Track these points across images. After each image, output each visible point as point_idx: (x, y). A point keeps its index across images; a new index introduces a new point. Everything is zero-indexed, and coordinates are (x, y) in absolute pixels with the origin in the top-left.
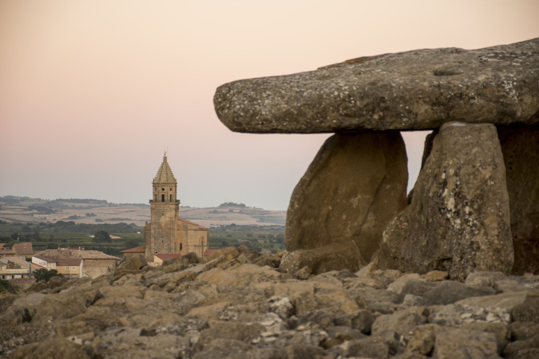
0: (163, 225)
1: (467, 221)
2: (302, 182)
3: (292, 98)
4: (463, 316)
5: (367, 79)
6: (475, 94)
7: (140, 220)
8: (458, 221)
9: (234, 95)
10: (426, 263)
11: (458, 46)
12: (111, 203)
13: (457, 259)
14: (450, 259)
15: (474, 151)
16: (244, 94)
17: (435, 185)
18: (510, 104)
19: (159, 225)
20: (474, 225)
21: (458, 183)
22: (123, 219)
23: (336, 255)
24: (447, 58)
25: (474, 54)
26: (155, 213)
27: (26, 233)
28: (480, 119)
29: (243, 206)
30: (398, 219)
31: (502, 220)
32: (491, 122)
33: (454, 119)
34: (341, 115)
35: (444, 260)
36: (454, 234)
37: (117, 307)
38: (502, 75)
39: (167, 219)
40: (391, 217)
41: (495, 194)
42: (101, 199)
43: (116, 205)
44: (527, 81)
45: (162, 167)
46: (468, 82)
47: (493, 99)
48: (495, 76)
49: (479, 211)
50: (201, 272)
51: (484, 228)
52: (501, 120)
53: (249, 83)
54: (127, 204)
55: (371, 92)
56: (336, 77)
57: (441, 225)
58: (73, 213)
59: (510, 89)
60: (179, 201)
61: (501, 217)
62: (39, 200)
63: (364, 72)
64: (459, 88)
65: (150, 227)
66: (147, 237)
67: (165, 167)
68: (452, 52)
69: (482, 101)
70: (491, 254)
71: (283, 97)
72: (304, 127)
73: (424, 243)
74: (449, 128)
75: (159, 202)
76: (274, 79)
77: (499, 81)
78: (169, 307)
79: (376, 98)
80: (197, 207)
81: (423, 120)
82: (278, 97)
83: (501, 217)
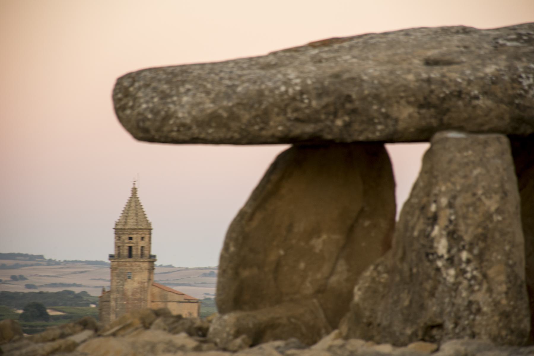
0: (129, 293)
1: (464, 272)
2: (242, 214)
3: (221, 95)
5: (330, 68)
6: (480, 93)
7: (94, 285)
8: (452, 272)
9: (139, 88)
10: (409, 331)
12: (50, 260)
13: (449, 325)
14: (440, 326)
15: (476, 172)
18: (529, 107)
19: (124, 294)
21: (453, 218)
22: (69, 285)
24: (449, 40)
25: (488, 35)
26: (118, 276)
28: (486, 128)
31: (513, 271)
33: (449, 127)
34: (289, 119)
35: (432, 327)
36: (446, 289)
38: (520, 66)
39: (136, 285)
40: (365, 268)
41: (503, 234)
42: (36, 253)
43: (58, 263)
45: (129, 204)
46: (470, 74)
50: (84, 341)
51: (488, 282)
53: (161, 72)
54: (76, 261)
55: (332, 88)
56: (286, 65)
57: (429, 277)
60: (154, 256)
61: (511, 266)
63: (327, 60)
64: (457, 84)
65: (109, 297)
66: (104, 313)
67: (134, 204)
68: (457, 32)
70: (497, 318)
71: (208, 93)
72: (237, 136)
73: (406, 303)
75: (124, 258)
76: (198, 67)
77: (513, 74)
79: (340, 96)
80: (184, 265)
82: (201, 92)
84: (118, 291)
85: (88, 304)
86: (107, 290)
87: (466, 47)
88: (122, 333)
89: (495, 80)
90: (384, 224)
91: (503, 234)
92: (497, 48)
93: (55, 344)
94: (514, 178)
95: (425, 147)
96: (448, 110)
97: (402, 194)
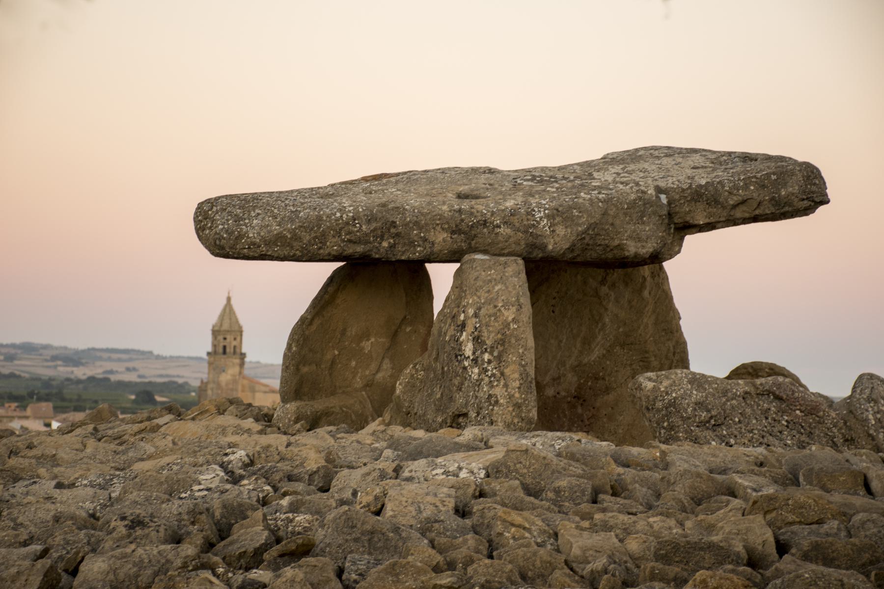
0: (223, 384)
1: (487, 371)
2: (303, 319)
4: (434, 472)
5: (378, 199)
7: (195, 376)
8: (476, 370)
9: (217, 212)
10: (440, 419)
11: (492, 166)
13: (473, 414)
14: (465, 415)
15: (497, 288)
16: (229, 212)
17: (452, 328)
19: (219, 385)
20: (493, 375)
22: (174, 376)
23: (341, 408)
25: (509, 175)
26: (214, 369)
27: (47, 391)
28: (506, 251)
30: (414, 367)
32: (519, 256)
33: (476, 250)
34: (343, 241)
35: (459, 416)
37: (45, 459)
38: (533, 201)
40: (407, 366)
43: (165, 358)
44: (560, 209)
45: (224, 310)
47: (522, 229)
48: (525, 202)
49: (499, 358)
52: (530, 253)
55: (380, 215)
57: (457, 375)
58: (109, 366)
59: (541, 218)
61: (523, 366)
62: (66, 348)
63: (376, 192)
64: (483, 215)
65: (206, 386)
67: (228, 310)
68: (484, 172)
69: (508, 231)
70: (511, 409)
72: (298, 253)
73: (438, 396)
74: (471, 260)
78: (109, 461)
79: (386, 222)
81: (441, 251)
83: (523, 366)
84: (214, 382)
85: (189, 392)
86: (205, 381)
87: (490, 185)
88: (199, 417)
89: (513, 213)
90: (422, 330)
92: (516, 186)
94: (528, 294)
95: (456, 266)
96: (475, 236)
97: (438, 305)
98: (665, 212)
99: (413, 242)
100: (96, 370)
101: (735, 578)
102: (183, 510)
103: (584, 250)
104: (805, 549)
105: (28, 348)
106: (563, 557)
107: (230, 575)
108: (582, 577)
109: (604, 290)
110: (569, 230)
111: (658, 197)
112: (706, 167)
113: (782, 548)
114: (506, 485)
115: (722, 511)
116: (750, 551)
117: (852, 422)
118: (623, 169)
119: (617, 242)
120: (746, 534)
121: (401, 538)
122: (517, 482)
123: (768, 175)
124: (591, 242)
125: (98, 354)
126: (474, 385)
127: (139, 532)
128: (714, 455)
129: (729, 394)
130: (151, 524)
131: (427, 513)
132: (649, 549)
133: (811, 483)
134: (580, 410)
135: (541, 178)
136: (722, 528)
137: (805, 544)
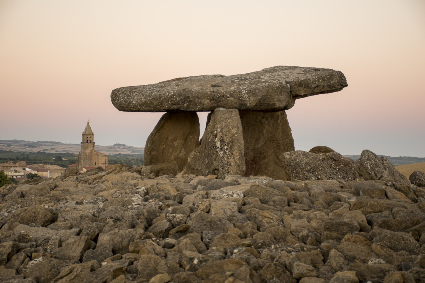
0: (87, 154)
1: (226, 152)
2: (152, 134)
4: (223, 195)
5: (182, 87)
7: (76, 151)
8: (222, 153)
10: (207, 171)
11: (222, 74)
13: (221, 169)
14: (218, 170)
15: (229, 121)
19: (86, 154)
20: (229, 154)
26: (84, 148)
27: (23, 157)
28: (231, 107)
29: (124, 145)
32: (236, 108)
33: (220, 107)
34: (170, 104)
35: (215, 170)
38: (241, 87)
39: (89, 151)
40: (192, 151)
41: (238, 140)
42: (58, 141)
43: (65, 144)
45: (87, 127)
47: (237, 98)
48: (238, 88)
49: (231, 148)
50: (104, 175)
52: (241, 107)
55: (183, 94)
57: (214, 154)
58: (45, 148)
59: (244, 94)
61: (240, 151)
62: (29, 141)
64: (222, 93)
67: (88, 127)
68: (219, 77)
69: (232, 99)
70: (236, 167)
71: (143, 95)
73: (207, 162)
78: (89, 191)
79: (186, 97)
80: (103, 145)
83: (240, 151)
89: (234, 92)
91: (238, 140)
93: (95, 176)
94: (241, 123)
96: (220, 101)
98: (289, 91)
99: (196, 104)
100: (40, 149)
101: (361, 237)
102: (134, 214)
103: (260, 106)
104: (380, 223)
105: (16, 142)
106: (289, 231)
107: (158, 240)
108: (298, 238)
109: (264, 120)
110: (255, 98)
111: (286, 85)
112: (302, 73)
113: (370, 223)
114: (253, 199)
115: (341, 208)
116: (360, 225)
117: (362, 168)
118: (271, 74)
119: (272, 102)
120: (355, 217)
121: (223, 224)
122: (258, 199)
123: (326, 76)
124: (263, 103)
125: (41, 143)
126: (221, 158)
127: (119, 223)
128: (325, 185)
129: (317, 159)
130: (123, 220)
131: (229, 213)
132: (321, 225)
133: (365, 195)
134: (254, 166)
135: (241, 79)
136: (345, 215)
137: (380, 221)
